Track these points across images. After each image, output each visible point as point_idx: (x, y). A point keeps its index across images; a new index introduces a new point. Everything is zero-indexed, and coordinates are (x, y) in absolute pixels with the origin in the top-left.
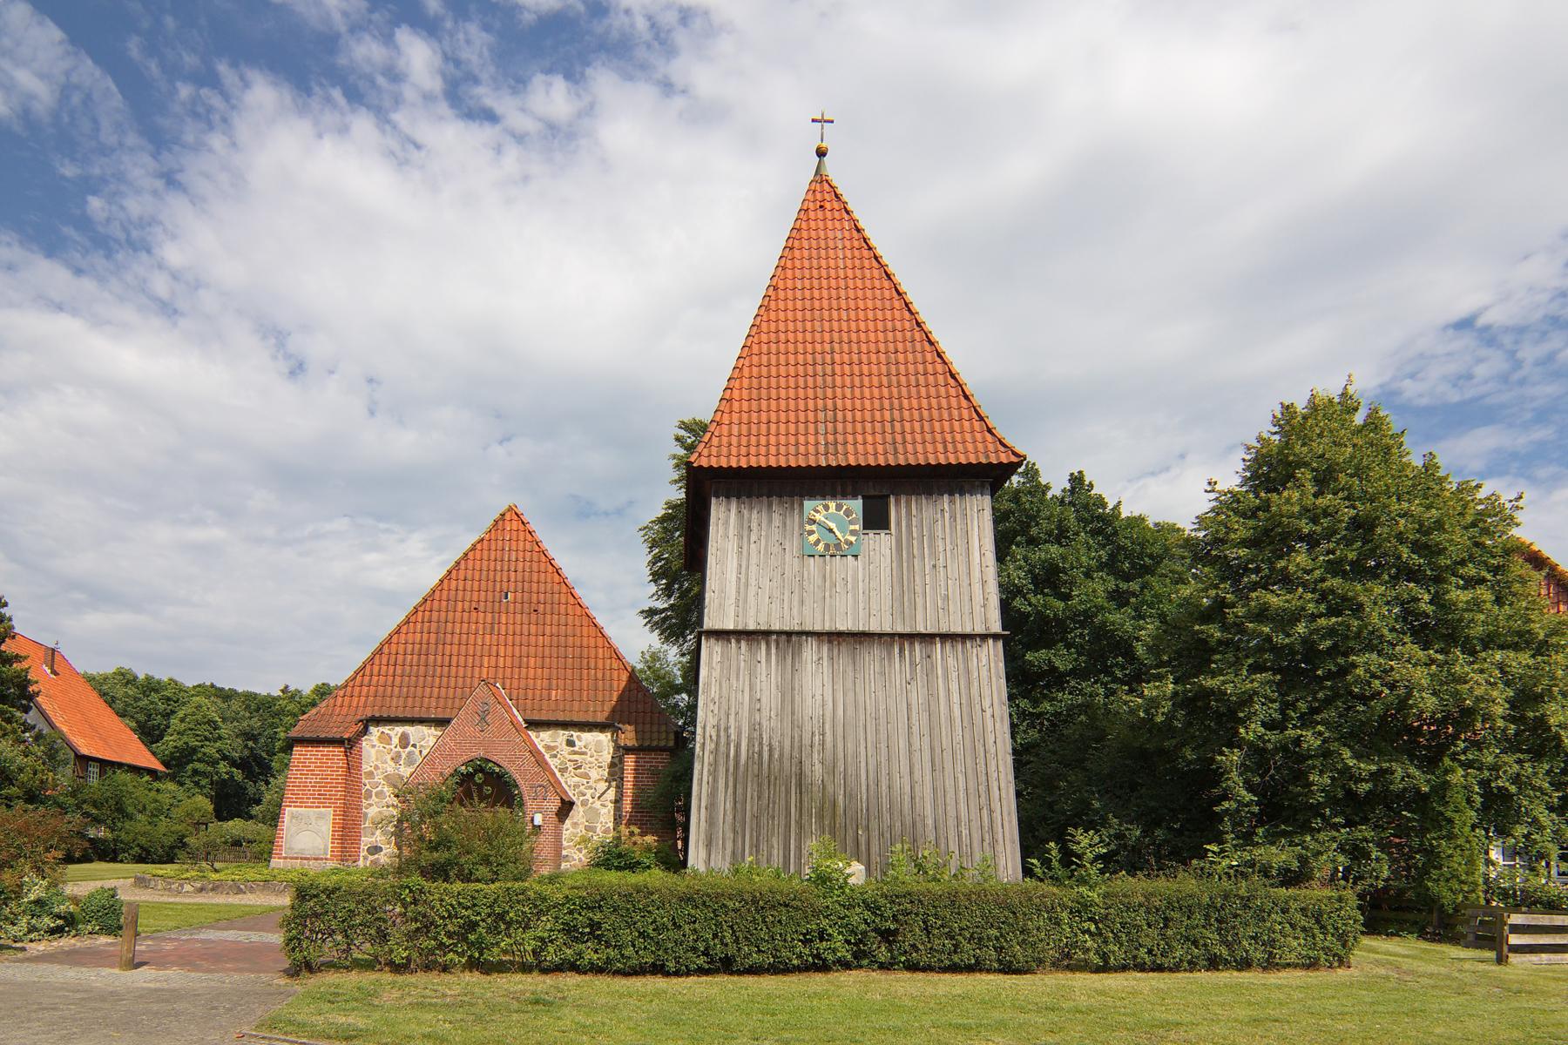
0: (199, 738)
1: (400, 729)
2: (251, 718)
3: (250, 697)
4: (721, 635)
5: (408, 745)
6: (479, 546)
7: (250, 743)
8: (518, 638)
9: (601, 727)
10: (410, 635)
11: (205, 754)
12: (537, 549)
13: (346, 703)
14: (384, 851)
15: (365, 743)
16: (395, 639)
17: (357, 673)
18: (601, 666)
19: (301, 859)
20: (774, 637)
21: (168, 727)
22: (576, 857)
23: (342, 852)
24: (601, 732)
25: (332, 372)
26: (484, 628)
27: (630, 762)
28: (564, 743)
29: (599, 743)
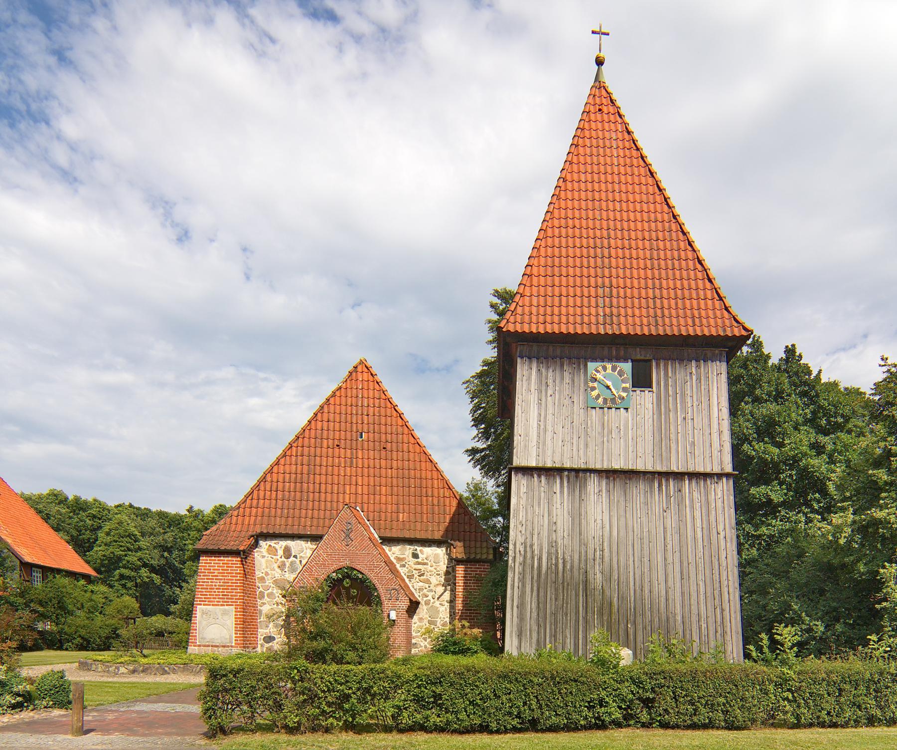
0: (123, 549)
1: (283, 543)
3: (162, 515)
4: (527, 471)
6: (338, 393)
7: (166, 554)
9: (438, 543)
10: (287, 467)
11: (128, 562)
12: (384, 397)
13: (240, 522)
14: (277, 640)
16: (275, 469)
17: (247, 497)
18: (436, 495)
19: (212, 646)
22: (422, 644)
24: (438, 547)
27: (460, 570)
28: (411, 555)
29: (436, 556)
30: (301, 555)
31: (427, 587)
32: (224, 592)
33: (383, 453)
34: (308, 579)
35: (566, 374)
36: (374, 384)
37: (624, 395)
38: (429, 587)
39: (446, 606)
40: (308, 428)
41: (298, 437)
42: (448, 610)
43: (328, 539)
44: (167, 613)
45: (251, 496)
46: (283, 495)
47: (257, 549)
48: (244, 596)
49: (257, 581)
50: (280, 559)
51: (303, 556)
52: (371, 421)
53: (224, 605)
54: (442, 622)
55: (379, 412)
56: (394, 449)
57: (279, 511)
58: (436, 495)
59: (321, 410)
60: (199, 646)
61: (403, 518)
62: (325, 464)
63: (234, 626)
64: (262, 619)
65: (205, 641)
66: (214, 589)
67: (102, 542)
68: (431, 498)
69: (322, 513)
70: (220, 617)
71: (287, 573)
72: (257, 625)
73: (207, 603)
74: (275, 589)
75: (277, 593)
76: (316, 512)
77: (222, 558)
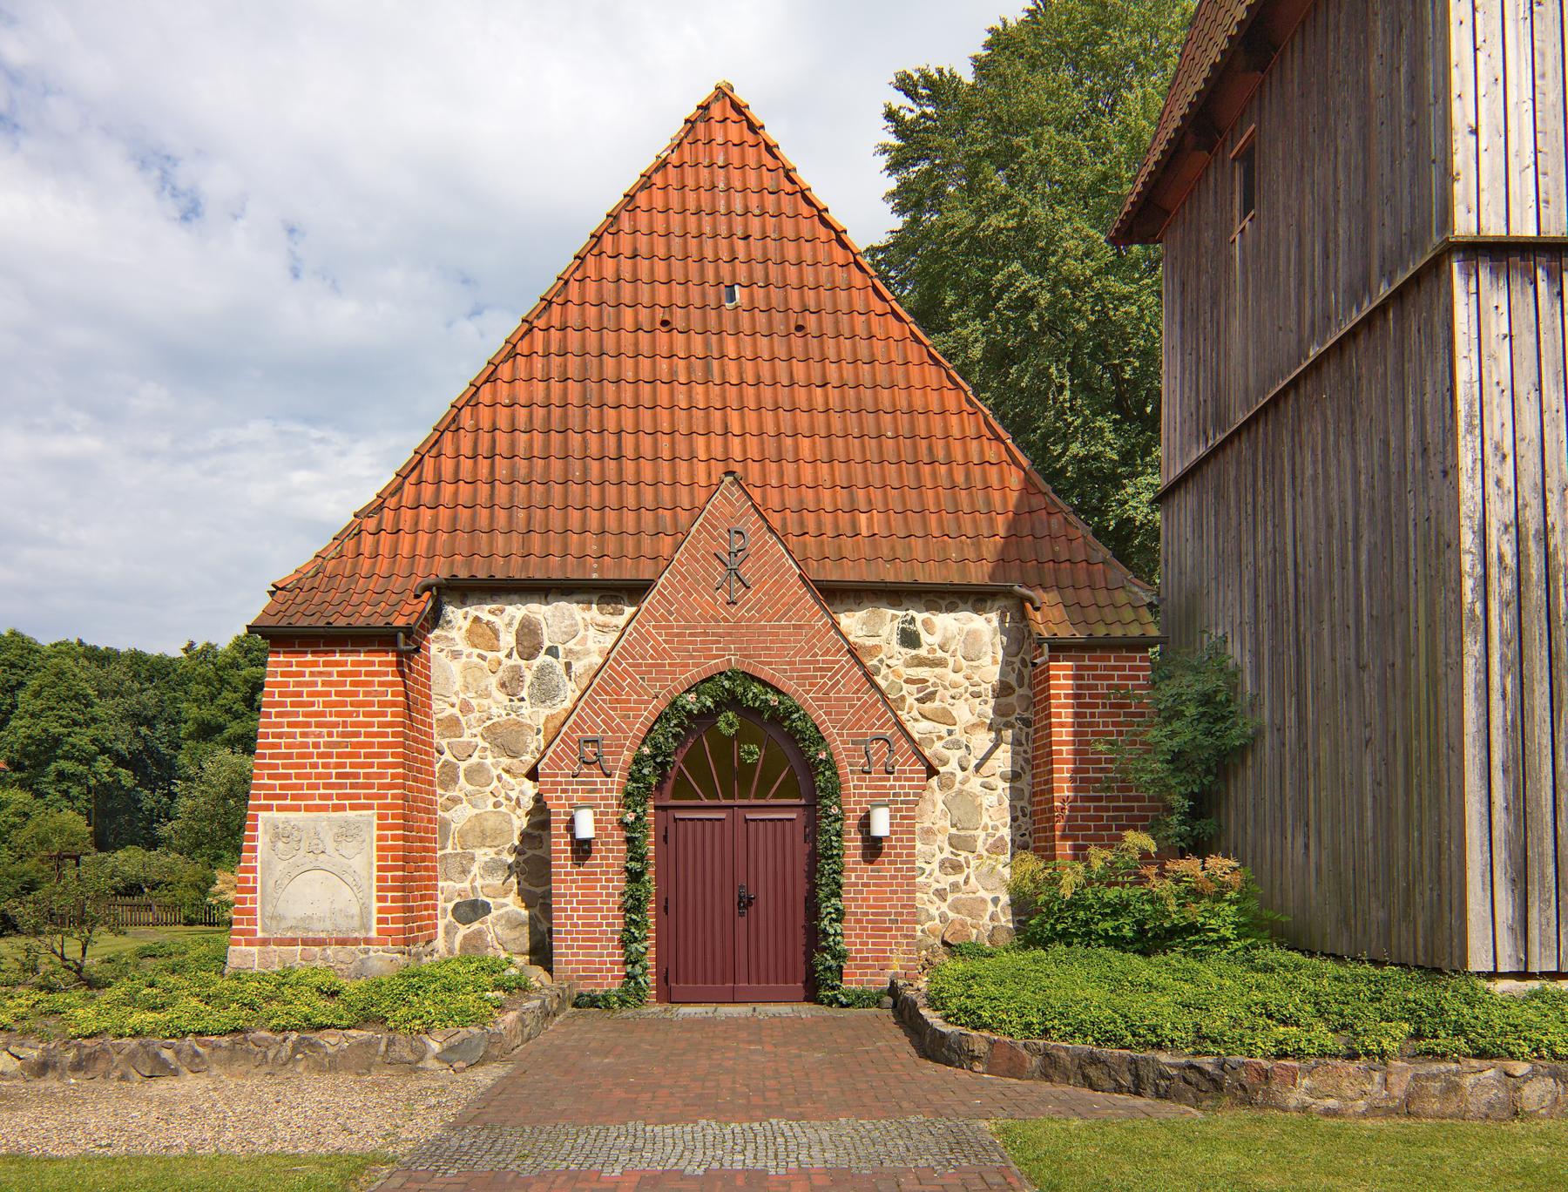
0: (64, 722)
1: (517, 611)
2: (142, 691)
3: (137, 657)
6: (658, 179)
7: (144, 730)
8: (767, 393)
10: (520, 386)
11: (73, 746)
12: (788, 187)
13: (385, 549)
14: (494, 913)
15: (436, 647)
16: (485, 395)
17: (402, 476)
18: (959, 457)
19: (305, 942)
21: (14, 706)
22: (934, 911)
23: (405, 921)
24: (976, 611)
25: (236, 217)
27: (1062, 677)
28: (895, 638)
29: (972, 637)
30: (570, 645)
31: (944, 733)
32: (343, 765)
33: (797, 342)
34: (608, 715)
36: (759, 150)
38: (950, 733)
39: (1000, 791)
40: (578, 275)
41: (550, 303)
42: (1007, 802)
43: (673, 586)
44: (152, 843)
45: (416, 473)
46: (513, 469)
47: (437, 632)
48: (405, 777)
49: (435, 731)
50: (505, 661)
51: (578, 648)
52: (757, 254)
53: (342, 808)
54: (990, 840)
55: (779, 228)
56: (829, 328)
57: (501, 516)
58: (960, 458)
59: (612, 225)
60: (264, 942)
62: (630, 376)
63: (375, 873)
64: (449, 850)
65: (283, 925)
66: (311, 755)
67: (26, 712)
68: (943, 469)
69: (630, 518)
70: (330, 846)
71: (526, 704)
72: (434, 869)
73: (288, 802)
74: (488, 753)
75: (496, 765)
76: (611, 516)
77: (338, 657)
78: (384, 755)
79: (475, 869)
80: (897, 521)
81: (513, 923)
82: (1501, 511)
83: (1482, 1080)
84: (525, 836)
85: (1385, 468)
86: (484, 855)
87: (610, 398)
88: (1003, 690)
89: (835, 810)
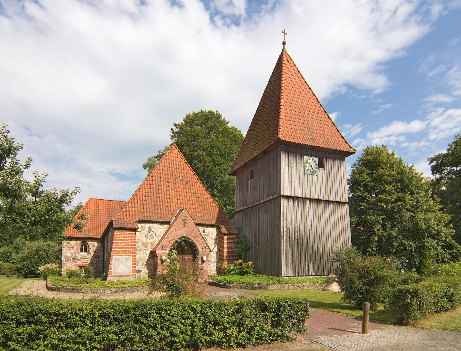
1: (148, 225)
4: (286, 197)
5: (151, 231)
8: (183, 193)
9: (212, 226)
19: (120, 276)
20: (299, 199)
26: (171, 189)
27: (225, 238)
29: (212, 232)
35: (297, 160)
37: (316, 170)
46: (146, 202)
53: (126, 255)
60: (113, 276)
61: (199, 215)
70: (124, 261)
77: (126, 232)
78: (133, 247)
79: (139, 265)
80: (202, 214)
81: (146, 273)
82: (285, 226)
83: (286, 286)
84: (148, 260)
85: (272, 218)
86: (141, 263)
87: (160, 192)
88: (216, 239)
89: (198, 257)
